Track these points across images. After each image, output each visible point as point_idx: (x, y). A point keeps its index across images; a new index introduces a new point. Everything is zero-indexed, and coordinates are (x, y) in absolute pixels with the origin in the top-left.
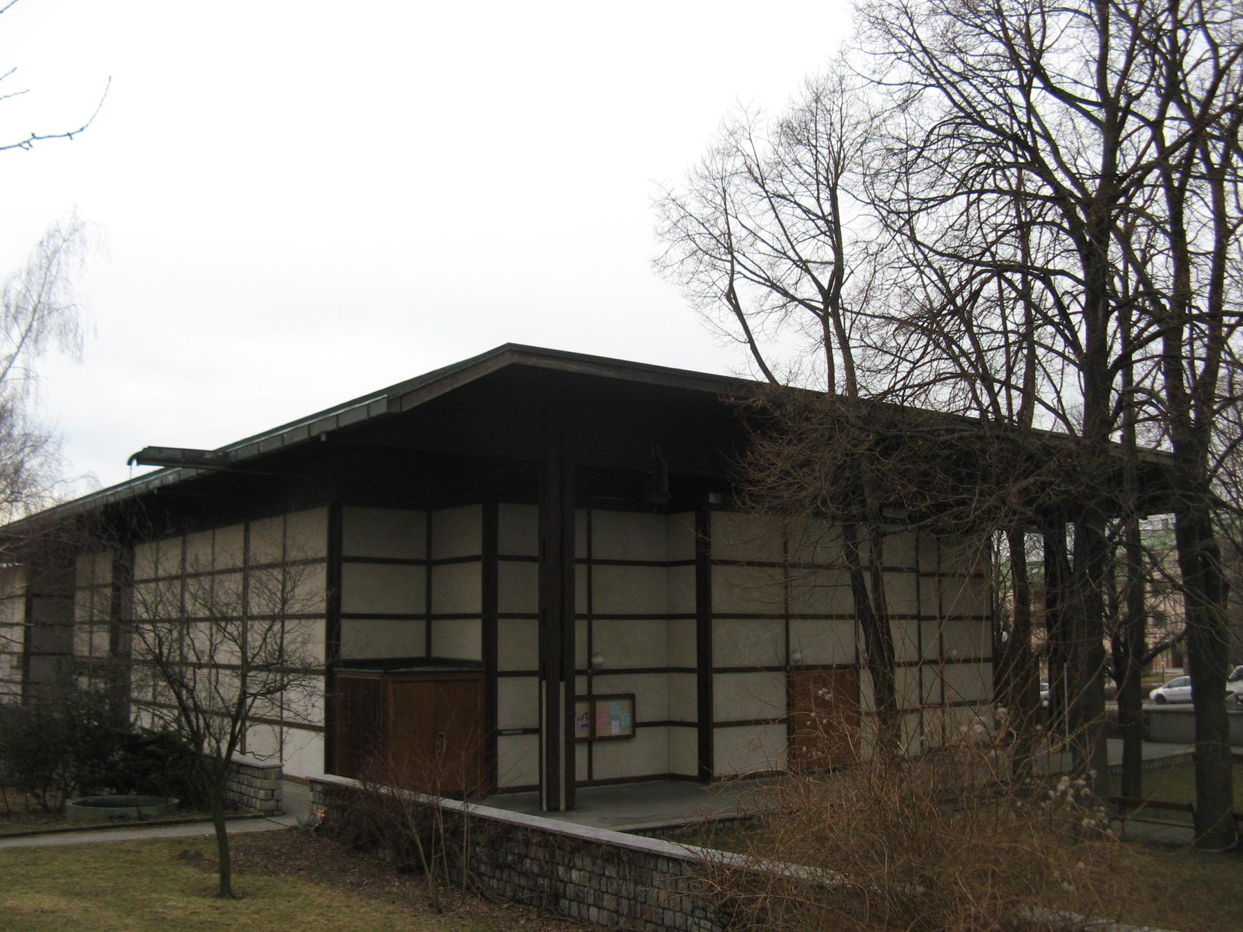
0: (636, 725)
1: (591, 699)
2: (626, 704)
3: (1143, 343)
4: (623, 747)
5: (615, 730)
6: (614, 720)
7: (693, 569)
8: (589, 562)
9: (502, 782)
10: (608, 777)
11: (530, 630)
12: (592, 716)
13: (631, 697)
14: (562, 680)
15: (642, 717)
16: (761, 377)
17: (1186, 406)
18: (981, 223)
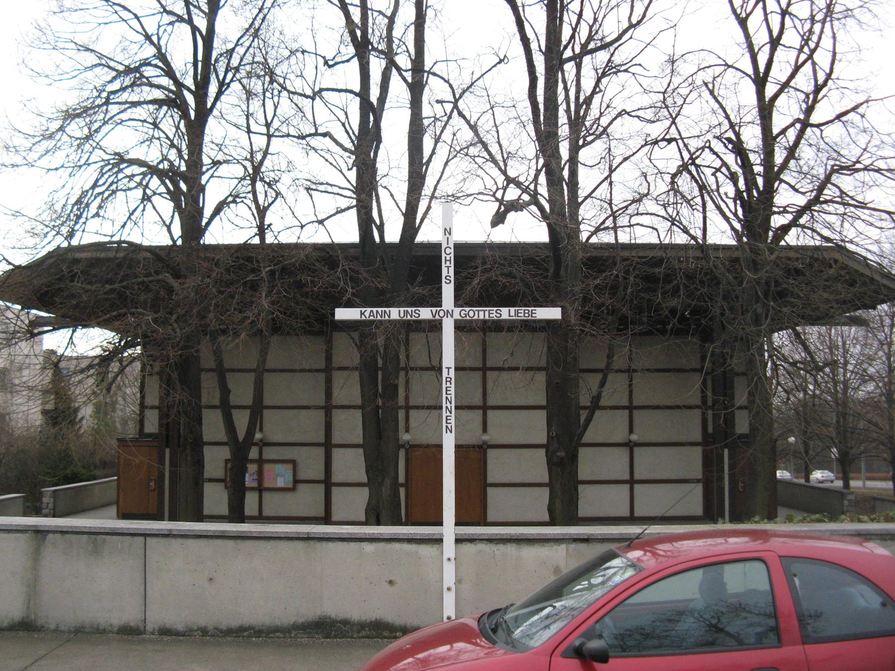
0: (296, 481)
1: (261, 461)
2: (290, 466)
3: (70, 220)
4: (288, 496)
5: (280, 483)
6: (280, 476)
7: (253, 375)
8: (405, 369)
9: (206, 512)
10: (275, 515)
11: (357, 417)
12: (260, 473)
13: (294, 462)
14: (167, 446)
15: (302, 476)
16: (11, 267)
17: (175, 248)
18: (151, 140)
